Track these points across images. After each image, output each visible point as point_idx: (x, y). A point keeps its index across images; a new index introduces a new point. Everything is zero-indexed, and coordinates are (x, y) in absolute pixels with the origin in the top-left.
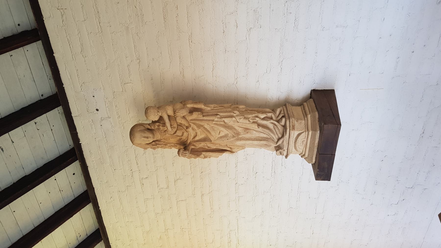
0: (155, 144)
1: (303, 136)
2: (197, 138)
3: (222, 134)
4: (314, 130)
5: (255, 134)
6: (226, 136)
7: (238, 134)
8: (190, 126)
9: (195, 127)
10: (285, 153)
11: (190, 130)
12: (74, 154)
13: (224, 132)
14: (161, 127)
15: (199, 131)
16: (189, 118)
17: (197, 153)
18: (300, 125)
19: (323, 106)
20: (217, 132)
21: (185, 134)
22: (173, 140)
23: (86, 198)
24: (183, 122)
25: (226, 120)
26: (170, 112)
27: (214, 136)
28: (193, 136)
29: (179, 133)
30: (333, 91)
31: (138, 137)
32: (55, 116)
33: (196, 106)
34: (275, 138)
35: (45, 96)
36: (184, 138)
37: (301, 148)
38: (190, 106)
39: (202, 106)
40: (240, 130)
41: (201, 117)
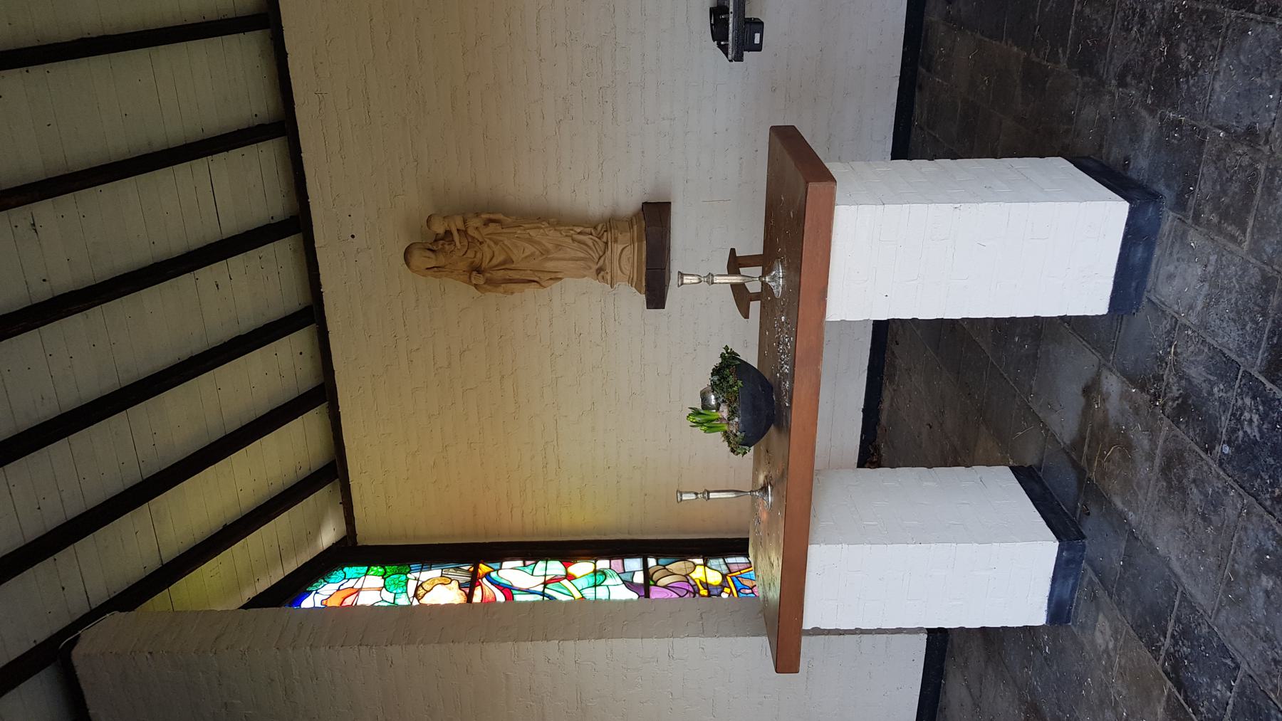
0: (437, 269)
1: (627, 254)
2: (495, 262)
3: (527, 253)
4: (640, 240)
5: (573, 254)
6: (532, 254)
7: (548, 252)
8: (543, 594)
9: (492, 244)
10: (609, 277)
11: (485, 248)
12: (310, 315)
13: (530, 249)
14: (447, 247)
15: (496, 249)
16: (485, 231)
17: (493, 283)
18: (624, 238)
19: (655, 217)
20: (521, 252)
21: (479, 255)
22: (463, 265)
23: (321, 394)
24: (476, 235)
25: (532, 233)
26: (460, 225)
27: (517, 255)
28: (488, 257)
29: (470, 254)
30: (877, 324)
31: (419, 258)
32: (282, 252)
33: (492, 216)
34: (596, 256)
35: (276, 220)
36: (477, 260)
37: (627, 267)
38: (485, 216)
39: (500, 217)
40: (550, 246)
41: (500, 230)
